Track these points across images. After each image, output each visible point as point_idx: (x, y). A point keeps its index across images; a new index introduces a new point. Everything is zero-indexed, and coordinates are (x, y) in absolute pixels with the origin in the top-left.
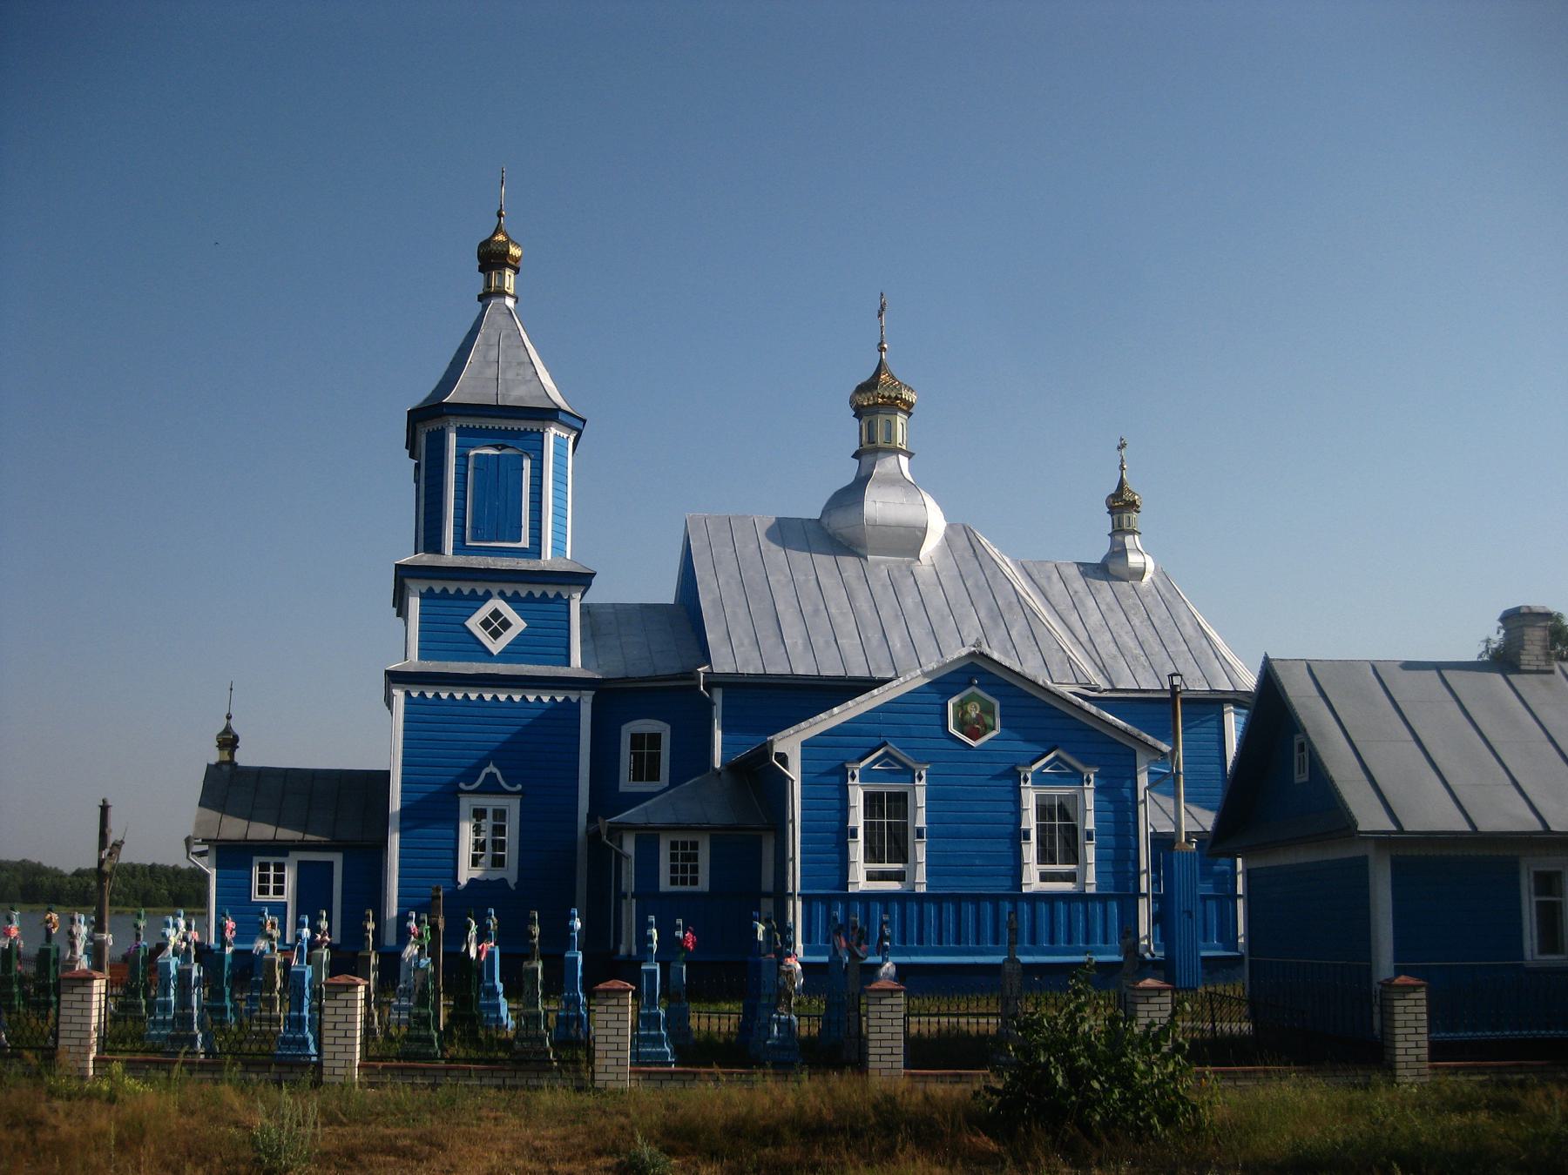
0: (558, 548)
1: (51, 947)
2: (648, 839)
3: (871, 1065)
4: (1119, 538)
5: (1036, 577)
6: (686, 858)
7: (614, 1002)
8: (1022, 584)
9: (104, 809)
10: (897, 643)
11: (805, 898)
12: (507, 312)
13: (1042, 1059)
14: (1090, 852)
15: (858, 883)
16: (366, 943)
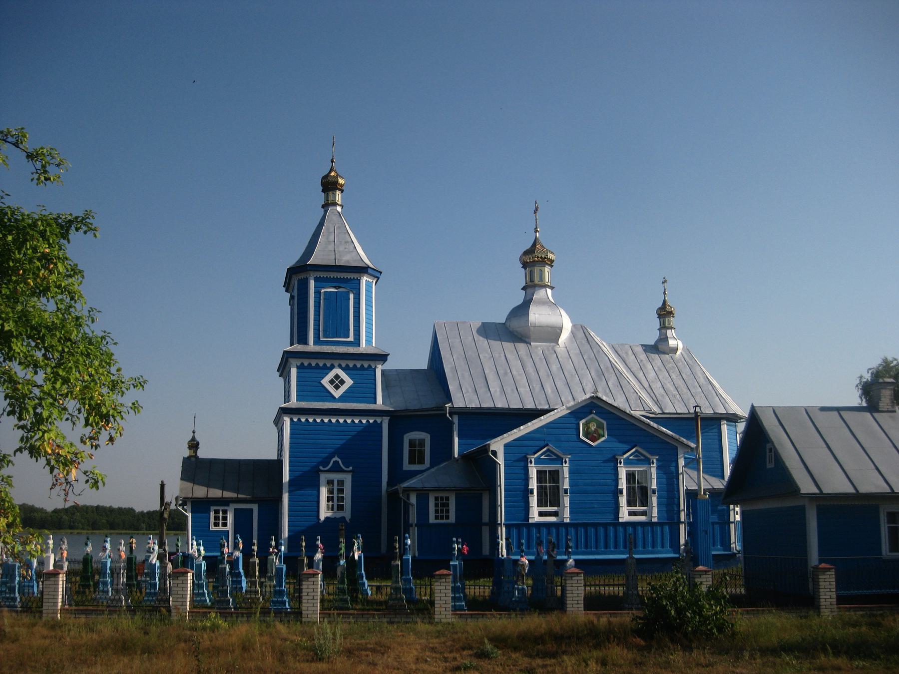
0: (369, 341)
1: (132, 556)
2: (423, 495)
3: (568, 609)
4: (663, 331)
5: (620, 353)
6: (443, 505)
7: (444, 580)
8: (613, 357)
9: (163, 486)
10: (549, 389)
11: (507, 526)
12: (338, 214)
13: (664, 603)
14: (654, 500)
15: (534, 518)
16: (302, 552)
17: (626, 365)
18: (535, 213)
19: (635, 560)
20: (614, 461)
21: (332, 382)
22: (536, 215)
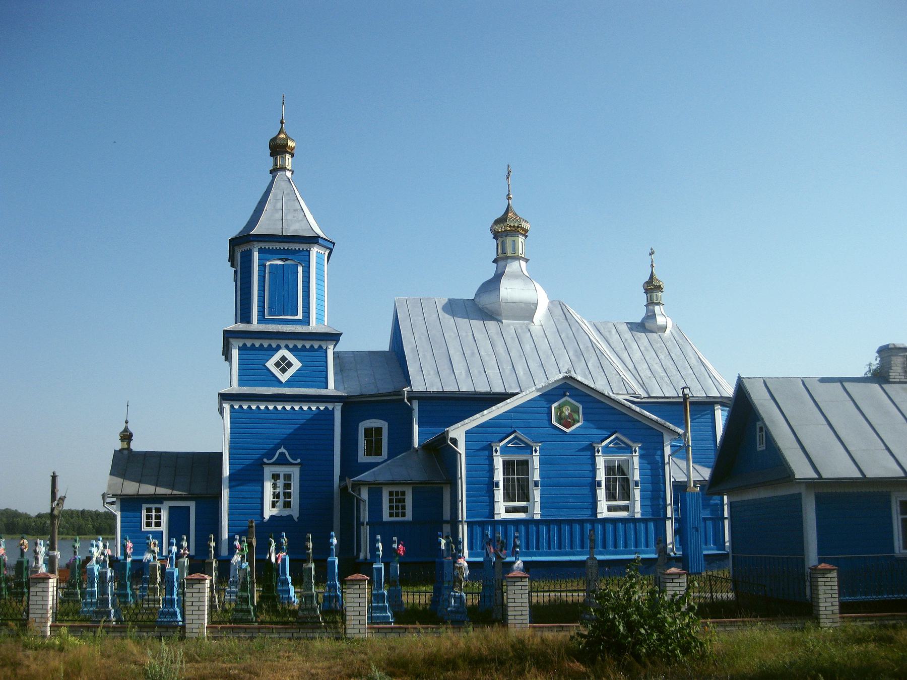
0: (320, 319)
2: (375, 490)
4: (651, 307)
6: (399, 501)
7: (357, 587)
9: (54, 478)
12: (287, 179)
13: (611, 617)
14: (637, 493)
17: (609, 344)
18: (508, 178)
19: (597, 562)
20: (591, 450)
21: (277, 365)
22: (508, 181)
